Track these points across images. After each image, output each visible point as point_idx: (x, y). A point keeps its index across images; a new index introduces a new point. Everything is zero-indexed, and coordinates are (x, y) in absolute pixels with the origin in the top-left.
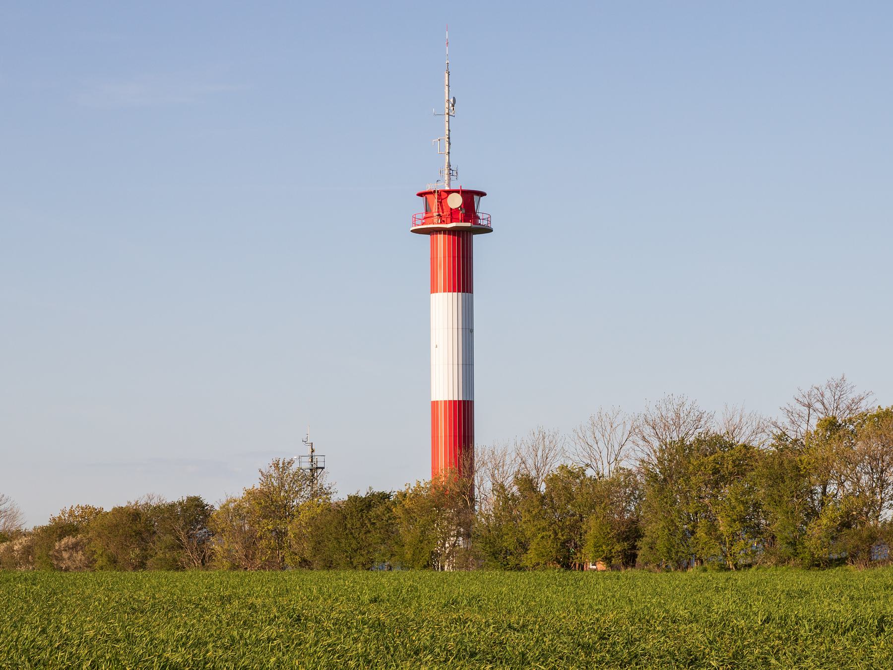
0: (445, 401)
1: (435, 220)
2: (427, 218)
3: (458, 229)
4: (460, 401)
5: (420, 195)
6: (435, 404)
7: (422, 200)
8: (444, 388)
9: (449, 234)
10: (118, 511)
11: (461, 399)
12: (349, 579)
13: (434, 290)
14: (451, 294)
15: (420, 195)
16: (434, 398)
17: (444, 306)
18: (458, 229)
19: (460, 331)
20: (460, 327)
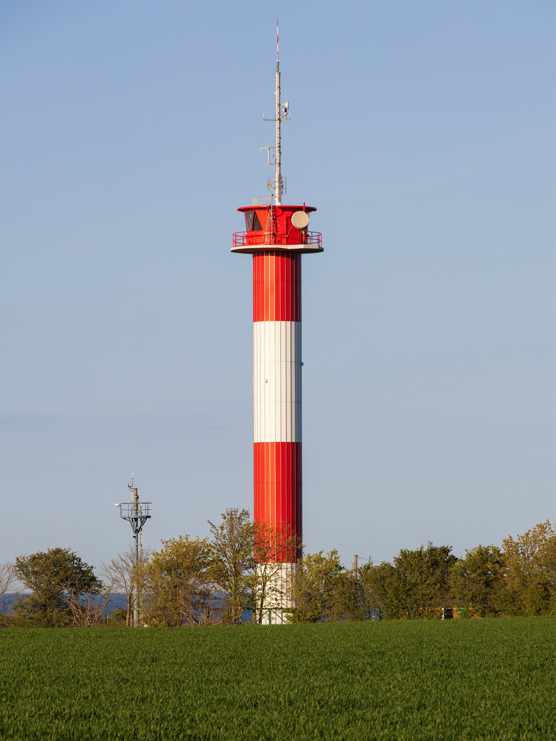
0: (277, 444)
1: (267, 240)
2: (250, 238)
3: (281, 252)
4: (288, 443)
5: (241, 210)
6: (259, 448)
7: (243, 214)
8: (271, 428)
9: (283, 256)
10: (408, 559)
11: (294, 441)
12: (404, 622)
13: (258, 316)
14: (278, 322)
15: (241, 210)
16: (259, 438)
17: (271, 337)
18: (281, 252)
19: (293, 364)
20: (293, 360)
